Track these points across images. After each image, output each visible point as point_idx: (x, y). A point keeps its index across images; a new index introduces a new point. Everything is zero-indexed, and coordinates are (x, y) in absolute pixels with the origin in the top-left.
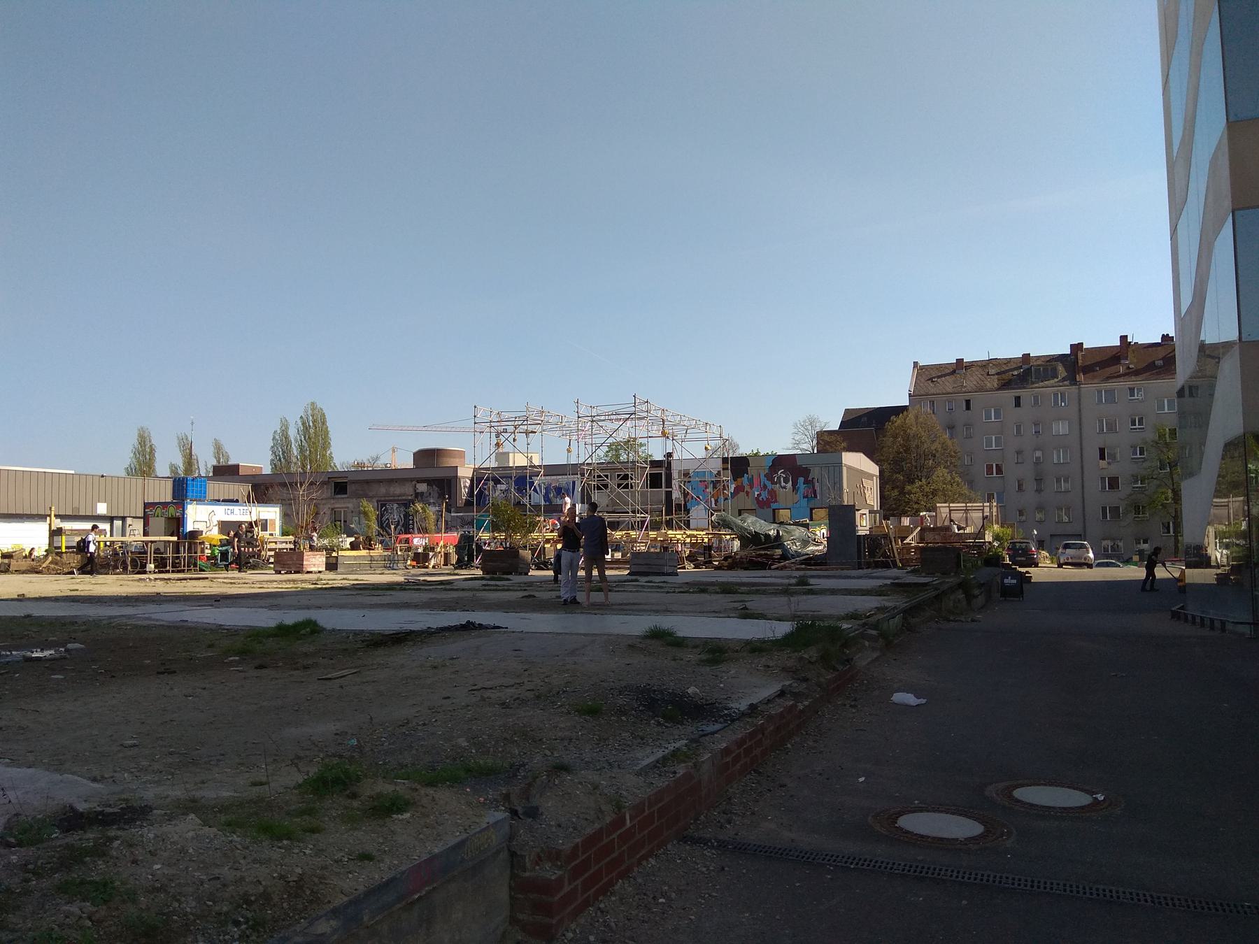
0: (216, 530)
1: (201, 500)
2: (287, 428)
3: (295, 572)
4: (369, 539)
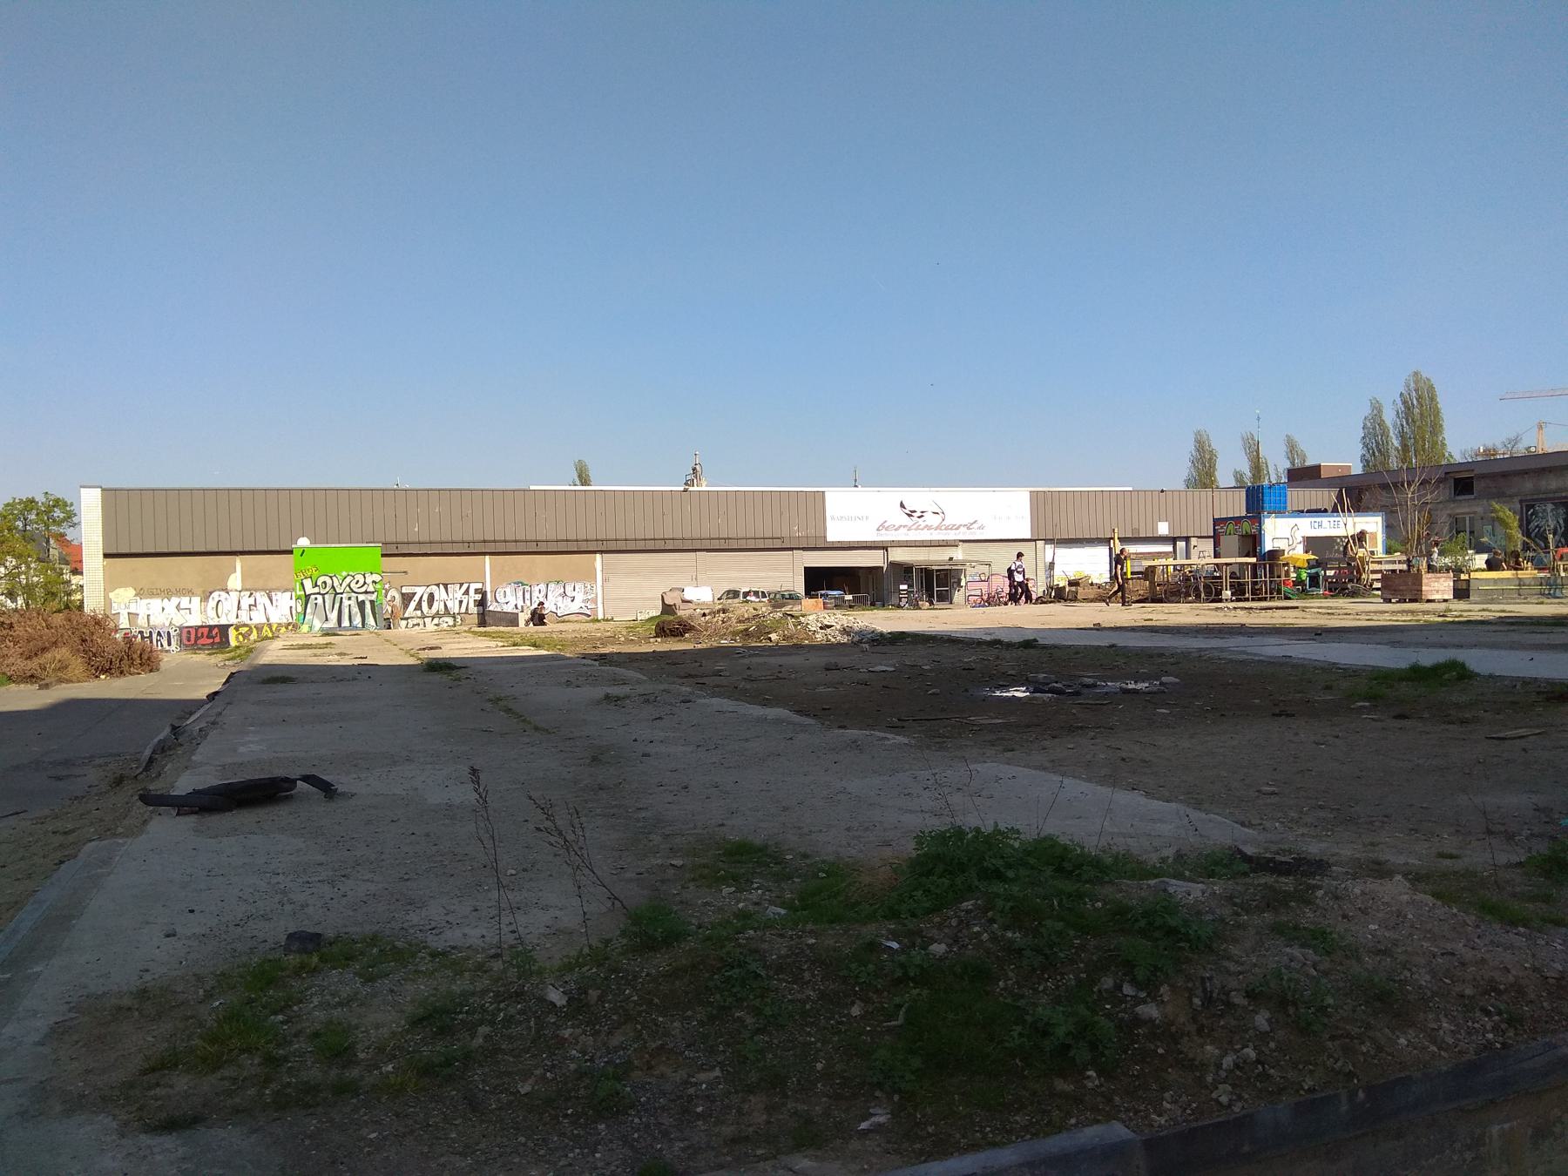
0: (1300, 549)
1: (1280, 512)
2: (1380, 411)
3: (1412, 601)
4: (1516, 555)
